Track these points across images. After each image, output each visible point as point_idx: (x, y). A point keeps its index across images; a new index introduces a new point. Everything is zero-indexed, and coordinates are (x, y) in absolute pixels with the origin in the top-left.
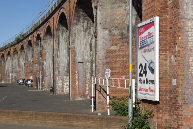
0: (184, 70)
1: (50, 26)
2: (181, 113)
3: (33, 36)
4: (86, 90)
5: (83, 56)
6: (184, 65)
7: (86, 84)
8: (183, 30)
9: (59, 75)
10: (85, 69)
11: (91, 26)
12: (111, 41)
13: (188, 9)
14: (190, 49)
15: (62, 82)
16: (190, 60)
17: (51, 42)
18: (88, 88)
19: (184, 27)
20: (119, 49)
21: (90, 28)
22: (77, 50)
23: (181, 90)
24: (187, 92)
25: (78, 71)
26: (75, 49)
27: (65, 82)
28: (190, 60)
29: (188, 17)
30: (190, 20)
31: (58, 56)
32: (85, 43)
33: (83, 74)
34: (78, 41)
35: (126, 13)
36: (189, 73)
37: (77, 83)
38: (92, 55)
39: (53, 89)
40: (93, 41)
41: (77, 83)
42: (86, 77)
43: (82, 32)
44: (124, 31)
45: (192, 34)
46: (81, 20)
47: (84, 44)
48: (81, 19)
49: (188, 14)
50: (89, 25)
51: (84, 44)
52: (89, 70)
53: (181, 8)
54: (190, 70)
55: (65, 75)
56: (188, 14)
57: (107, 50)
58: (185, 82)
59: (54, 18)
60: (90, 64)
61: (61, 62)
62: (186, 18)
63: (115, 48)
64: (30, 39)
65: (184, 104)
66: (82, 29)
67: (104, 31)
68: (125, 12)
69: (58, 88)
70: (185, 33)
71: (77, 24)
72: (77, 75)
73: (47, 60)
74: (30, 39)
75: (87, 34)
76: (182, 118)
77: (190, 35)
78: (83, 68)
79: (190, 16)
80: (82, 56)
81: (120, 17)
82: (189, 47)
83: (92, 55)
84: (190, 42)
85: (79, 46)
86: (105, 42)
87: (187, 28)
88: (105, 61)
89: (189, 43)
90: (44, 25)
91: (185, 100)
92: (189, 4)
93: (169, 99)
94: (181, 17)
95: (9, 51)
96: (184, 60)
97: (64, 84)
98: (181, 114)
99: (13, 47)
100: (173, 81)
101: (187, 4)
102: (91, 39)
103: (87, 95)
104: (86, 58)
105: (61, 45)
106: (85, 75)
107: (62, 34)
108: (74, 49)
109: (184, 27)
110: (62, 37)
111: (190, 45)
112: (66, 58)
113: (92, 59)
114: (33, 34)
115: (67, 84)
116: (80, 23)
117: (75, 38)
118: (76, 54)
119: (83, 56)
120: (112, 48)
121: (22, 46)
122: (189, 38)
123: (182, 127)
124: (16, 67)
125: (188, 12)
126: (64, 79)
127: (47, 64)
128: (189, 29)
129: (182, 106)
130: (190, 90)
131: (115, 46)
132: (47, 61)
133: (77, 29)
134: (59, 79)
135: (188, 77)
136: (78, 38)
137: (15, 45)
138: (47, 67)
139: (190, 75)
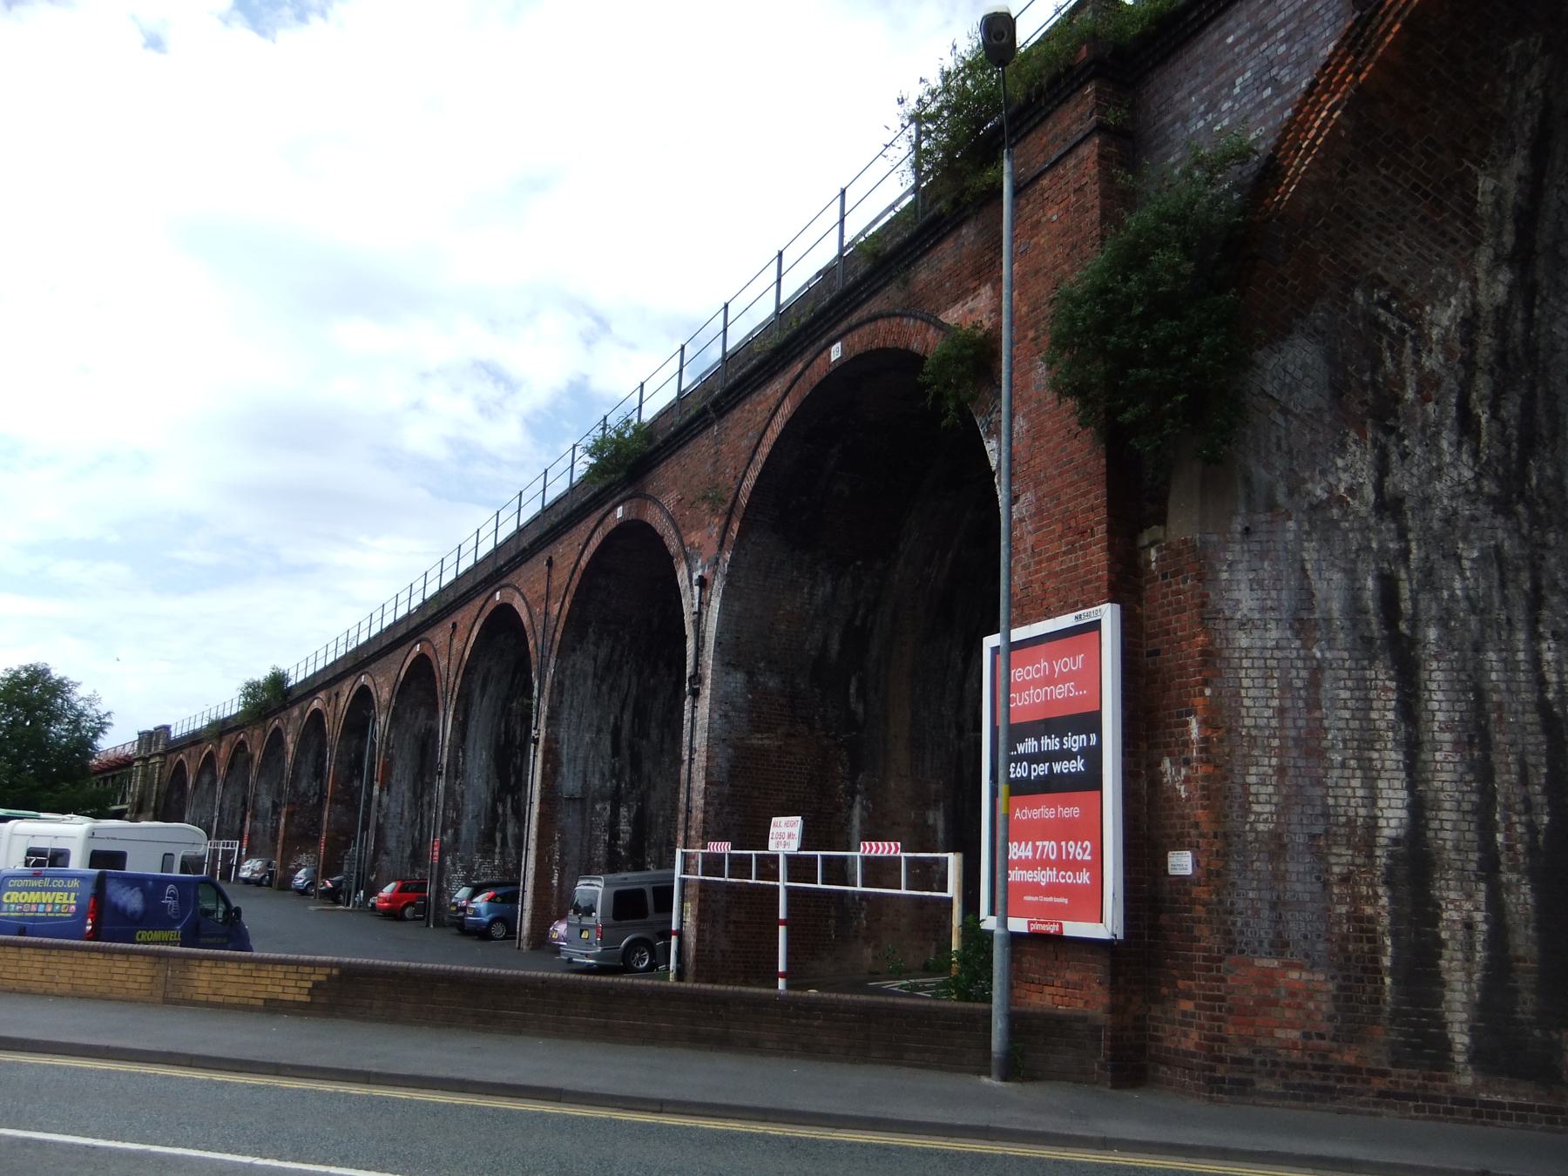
0: (1226, 816)
1: (373, 689)
2: (1219, 990)
3: (337, 695)
5: (585, 776)
6: (1226, 798)
8: (1218, 662)
9: (457, 850)
10: (587, 825)
11: (624, 659)
12: (752, 712)
13: (1234, 583)
14: (1249, 734)
16: (1252, 779)
17: (417, 717)
19: (1222, 649)
20: (780, 747)
22: (565, 747)
23: (1218, 895)
24: (1240, 905)
25: (562, 831)
28: (1252, 779)
29: (1238, 616)
30: (1245, 624)
31: (457, 771)
32: (595, 723)
33: (582, 845)
34: (570, 714)
35: (812, 612)
36: (1247, 827)
37: (555, 881)
38: (617, 771)
39: (425, 904)
40: (625, 717)
41: (555, 881)
43: (590, 682)
44: (798, 681)
45: (1253, 679)
48: (590, 630)
49: (1238, 601)
50: (616, 657)
52: (605, 831)
53: (1209, 577)
54: (1252, 818)
56: (1238, 601)
57: (735, 748)
58: (1233, 866)
59: (454, 625)
60: (609, 808)
61: (466, 796)
62: (1232, 619)
63: (767, 742)
65: (1229, 951)
66: (590, 670)
67: (727, 674)
68: (807, 607)
70: (1230, 674)
71: (574, 650)
73: (394, 789)
74: (316, 704)
75: (604, 688)
76: (1220, 1010)
77: (1246, 683)
78: (583, 819)
79: (1245, 611)
80: (581, 775)
81: (788, 627)
82: (1244, 727)
83: (617, 771)
84: (1248, 708)
85: (573, 733)
86: (730, 714)
87: (1237, 655)
88: (726, 790)
89: (1244, 712)
90: (399, 651)
91: (1231, 937)
92: (1240, 566)
93: (1146, 932)
94: (1208, 613)
95: (210, 753)
96: (1226, 778)
98: (1217, 993)
99: (233, 736)
100: (1170, 859)
101: (1230, 566)
104: (595, 781)
106: (589, 852)
107: (484, 687)
109: (1222, 649)
110: (479, 701)
111: (1248, 722)
112: (488, 783)
113: (618, 786)
114: (334, 690)
117: (561, 702)
119: (585, 776)
120: (756, 740)
122: (1243, 693)
123: (1223, 1045)
124: (234, 817)
125: (1236, 595)
127: (393, 805)
128: (1241, 659)
129: (1221, 960)
130: (1251, 895)
131: (765, 735)
132: (394, 794)
133: (574, 666)
134: (454, 864)
135: (1245, 846)
136: (572, 702)
138: (391, 815)
139: (1251, 837)
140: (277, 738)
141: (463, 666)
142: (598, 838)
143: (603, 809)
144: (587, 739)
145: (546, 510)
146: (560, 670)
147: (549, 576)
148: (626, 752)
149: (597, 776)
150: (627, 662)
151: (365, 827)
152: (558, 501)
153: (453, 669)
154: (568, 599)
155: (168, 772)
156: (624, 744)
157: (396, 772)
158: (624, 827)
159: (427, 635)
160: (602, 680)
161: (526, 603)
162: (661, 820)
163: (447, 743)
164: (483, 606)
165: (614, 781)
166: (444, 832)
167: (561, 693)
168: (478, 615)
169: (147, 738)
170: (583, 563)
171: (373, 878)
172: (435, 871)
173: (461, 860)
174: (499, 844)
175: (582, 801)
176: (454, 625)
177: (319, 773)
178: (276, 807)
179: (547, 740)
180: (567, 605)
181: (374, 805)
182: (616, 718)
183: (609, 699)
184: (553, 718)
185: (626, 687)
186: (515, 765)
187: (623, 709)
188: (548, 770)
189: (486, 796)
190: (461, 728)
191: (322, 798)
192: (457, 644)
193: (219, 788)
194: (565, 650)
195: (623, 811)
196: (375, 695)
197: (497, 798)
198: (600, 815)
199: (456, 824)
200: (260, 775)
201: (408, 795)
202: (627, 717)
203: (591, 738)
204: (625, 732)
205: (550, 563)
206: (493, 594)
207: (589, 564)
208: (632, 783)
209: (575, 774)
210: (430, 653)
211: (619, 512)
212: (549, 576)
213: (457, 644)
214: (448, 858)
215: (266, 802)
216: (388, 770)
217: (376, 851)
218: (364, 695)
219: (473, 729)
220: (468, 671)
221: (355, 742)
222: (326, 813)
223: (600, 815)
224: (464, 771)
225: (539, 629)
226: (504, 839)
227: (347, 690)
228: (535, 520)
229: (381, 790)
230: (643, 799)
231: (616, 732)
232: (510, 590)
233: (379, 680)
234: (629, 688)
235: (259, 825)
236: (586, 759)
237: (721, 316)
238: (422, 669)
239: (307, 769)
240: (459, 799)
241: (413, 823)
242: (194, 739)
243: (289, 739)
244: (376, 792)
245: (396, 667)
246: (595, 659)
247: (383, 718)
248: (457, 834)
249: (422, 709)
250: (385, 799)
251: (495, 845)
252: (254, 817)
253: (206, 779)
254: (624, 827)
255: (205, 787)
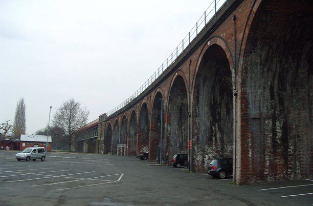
1: (162, 93)
4: (265, 168)
7: (265, 155)
9: (198, 144)
10: (262, 130)
15: (202, 154)
18: (268, 164)
21: (272, 60)
22: (250, 96)
25: (252, 133)
26: (246, 94)
27: (207, 154)
32: (262, 85)
34: (251, 82)
37: (250, 155)
40: (275, 82)
41: (250, 155)
42: (265, 145)
43: (259, 67)
46: (259, 45)
47: (260, 86)
51: (260, 86)
52: (270, 132)
55: (207, 144)
60: (271, 122)
64: (145, 102)
66: (258, 61)
69: (196, 162)
71: (251, 52)
72: (250, 140)
75: (265, 69)
80: (258, 108)
97: (205, 157)
102: (272, 79)
103: (267, 176)
104: (265, 111)
105: (201, 99)
108: (245, 96)
112: (208, 119)
113: (275, 112)
115: (209, 157)
116: (256, 50)
117: (247, 77)
118: (249, 104)
121: (235, 17)
126: (205, 149)
136: (251, 76)
137: (123, 112)
140: (134, 113)
141: (196, 75)
142: (267, 135)
143: (269, 122)
144: (259, 92)
145: (190, 44)
146: (245, 62)
147: (235, 24)
148: (276, 97)
149: (265, 109)
150: (275, 57)
151: (163, 138)
152: (181, 55)
153: (192, 77)
154: (247, 29)
155: (107, 126)
156: (276, 94)
157: (172, 119)
158: (278, 130)
159: (180, 68)
160: (264, 66)
161: (224, 40)
162: (294, 127)
163: (192, 104)
164: (202, 49)
165: (273, 111)
166: (193, 137)
167: (246, 73)
168: (200, 54)
169: (101, 117)
170: (255, 10)
171: (167, 155)
172: (191, 152)
173: (200, 147)
174: (214, 142)
175: (259, 119)
176: (191, 61)
177: (147, 123)
178: (135, 134)
179: (242, 93)
180: (247, 32)
181: (165, 130)
182: (271, 83)
183: (268, 75)
184: (243, 84)
185: (275, 68)
186: (218, 111)
187: (274, 79)
188: (243, 107)
189: (208, 124)
190: (197, 99)
191: (148, 129)
192: (192, 68)
193: (120, 129)
194: (247, 53)
195: (278, 123)
196: (162, 94)
197: (212, 124)
198: (267, 125)
199: (197, 134)
200: (130, 124)
201: (177, 126)
202: (276, 82)
203: (261, 92)
204: (275, 89)
205: (235, 18)
206: (207, 43)
207: (258, 9)
208: (280, 110)
209: (255, 108)
210: (181, 74)
211: (209, 43)
212: (235, 24)
213: (192, 68)
214: (195, 147)
215: (132, 132)
216: (169, 118)
217: (167, 146)
218: (159, 95)
219: (201, 99)
220: (198, 76)
221: (157, 111)
222: (150, 134)
223: (267, 125)
224: (199, 114)
225: (232, 49)
226: (216, 139)
227: (153, 94)
228: (188, 47)
229: (167, 125)
230: (286, 117)
231: (272, 88)
232: (214, 39)
233: (164, 89)
234: (276, 70)
235: (131, 139)
236: (260, 101)
237: (182, 43)
238: (180, 81)
239: (143, 122)
240: (198, 125)
241: (179, 136)
242: (114, 116)
243: (137, 112)
244: (166, 126)
245: (169, 83)
246: (261, 56)
247: (166, 101)
248: (198, 138)
249: (179, 97)
250: (169, 128)
251: (213, 141)
252: (130, 137)
253: (116, 127)
254: (278, 130)
255: (116, 130)
